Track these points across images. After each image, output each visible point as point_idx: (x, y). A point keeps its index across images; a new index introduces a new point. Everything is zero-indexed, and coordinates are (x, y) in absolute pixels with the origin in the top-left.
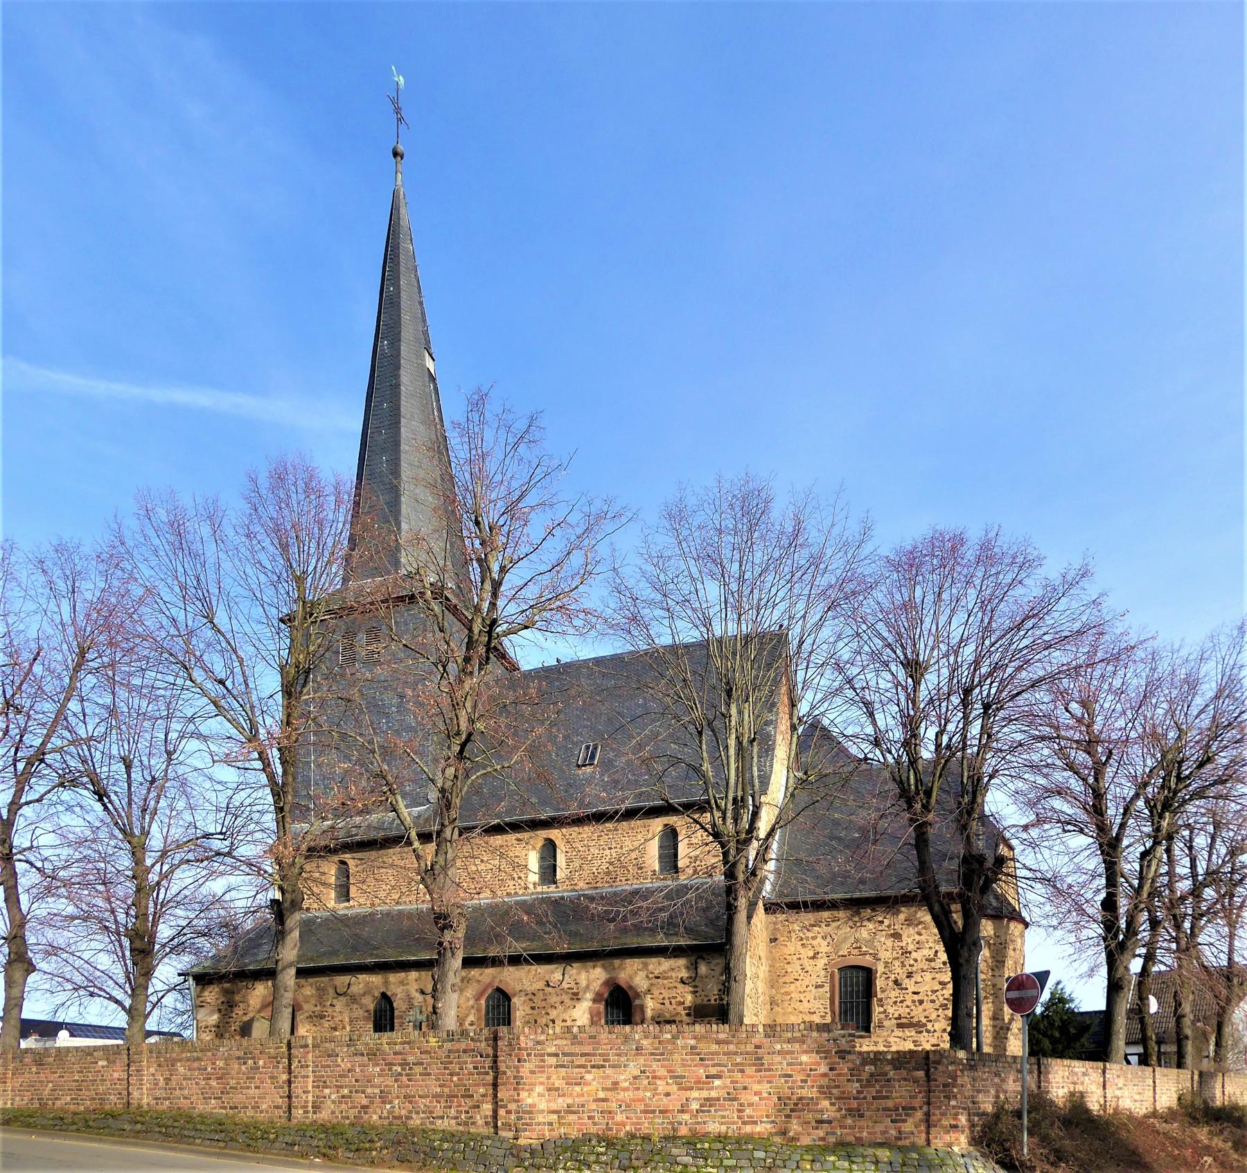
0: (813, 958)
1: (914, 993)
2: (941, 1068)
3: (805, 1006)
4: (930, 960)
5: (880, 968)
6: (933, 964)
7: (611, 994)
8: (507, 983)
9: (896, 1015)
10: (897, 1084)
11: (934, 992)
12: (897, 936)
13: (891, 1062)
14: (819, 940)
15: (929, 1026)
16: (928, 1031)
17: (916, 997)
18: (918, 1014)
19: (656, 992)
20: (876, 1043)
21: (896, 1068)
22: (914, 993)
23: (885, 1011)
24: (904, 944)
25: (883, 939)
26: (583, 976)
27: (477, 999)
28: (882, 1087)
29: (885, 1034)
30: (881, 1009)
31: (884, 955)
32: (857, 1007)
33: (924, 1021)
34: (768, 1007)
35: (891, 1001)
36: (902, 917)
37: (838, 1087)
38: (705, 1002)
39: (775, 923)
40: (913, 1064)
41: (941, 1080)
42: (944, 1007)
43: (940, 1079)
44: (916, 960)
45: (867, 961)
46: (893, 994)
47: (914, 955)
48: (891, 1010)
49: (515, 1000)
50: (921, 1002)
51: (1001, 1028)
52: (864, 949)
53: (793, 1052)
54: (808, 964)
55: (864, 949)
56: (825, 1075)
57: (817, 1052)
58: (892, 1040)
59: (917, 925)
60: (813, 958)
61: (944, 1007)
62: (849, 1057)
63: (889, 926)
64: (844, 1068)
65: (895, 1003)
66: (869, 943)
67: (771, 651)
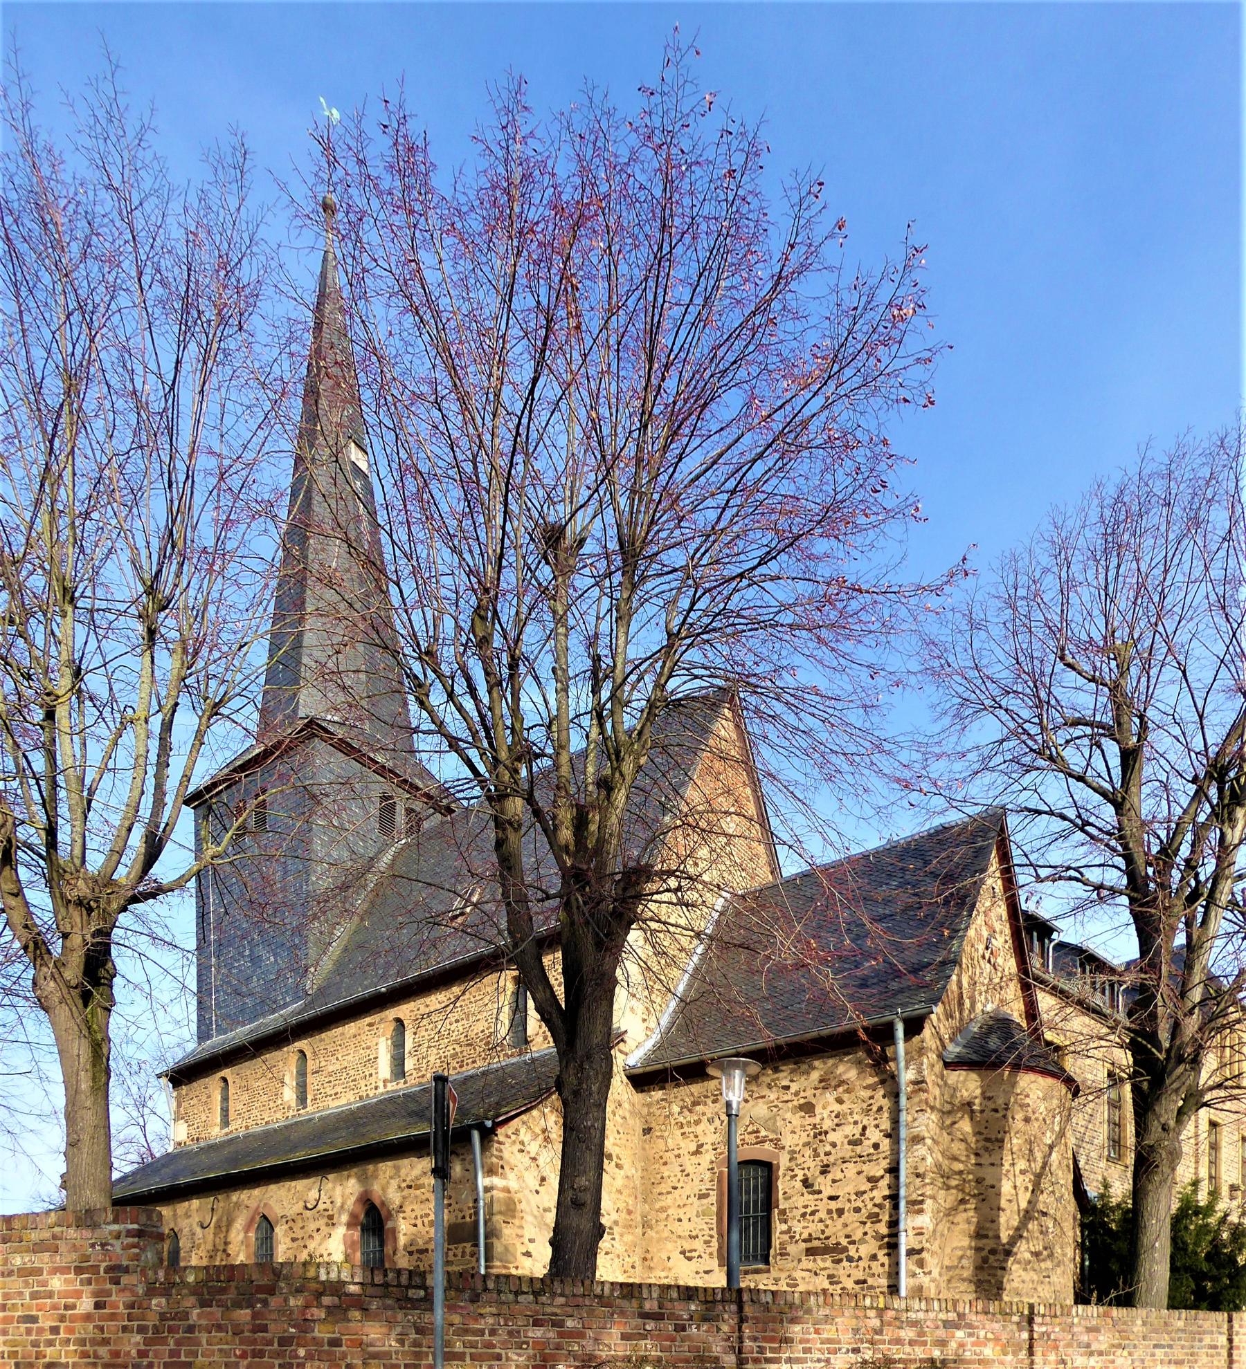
0: (697, 1152)
1: (831, 1198)
2: (274, 1302)
4: (854, 1143)
5: (783, 1161)
6: (858, 1149)
7: (367, 1214)
8: (271, 1208)
9: (805, 1236)
10: (204, 1337)
11: (859, 1194)
12: (808, 1108)
13: (196, 1290)
14: (704, 1125)
15: (852, 1251)
16: (850, 1259)
17: (834, 1205)
18: (836, 1232)
19: (407, 1208)
20: (777, 1280)
21: (204, 1304)
22: (831, 1198)
23: (789, 1231)
24: (817, 1120)
25: (789, 1116)
26: (339, 1190)
27: (246, 1232)
28: (178, 1343)
29: (790, 1265)
30: (784, 1227)
31: (788, 1141)
32: (755, 1224)
33: (844, 1242)
34: (639, 1230)
35: (797, 1213)
36: (815, 1075)
37: (106, 1342)
38: (460, 1221)
39: (649, 1105)
40: (232, 1294)
41: (275, 1330)
42: (874, 1218)
43: (271, 1327)
44: (834, 1145)
45: (764, 1152)
46: (800, 1201)
47: (832, 1137)
48: (797, 1228)
49: (277, 1230)
50: (840, 1212)
51: (993, 1252)
52: (763, 1133)
53: (39, 1271)
54: (689, 1163)
55: (763, 1133)
56: (87, 1317)
57: (79, 1270)
58: (798, 1274)
59: (836, 1087)
60: (697, 1152)
61: (874, 1218)
62: (125, 1280)
63: (797, 1094)
64: (119, 1300)
65: (804, 1215)
66: (770, 1123)
67: (988, 836)
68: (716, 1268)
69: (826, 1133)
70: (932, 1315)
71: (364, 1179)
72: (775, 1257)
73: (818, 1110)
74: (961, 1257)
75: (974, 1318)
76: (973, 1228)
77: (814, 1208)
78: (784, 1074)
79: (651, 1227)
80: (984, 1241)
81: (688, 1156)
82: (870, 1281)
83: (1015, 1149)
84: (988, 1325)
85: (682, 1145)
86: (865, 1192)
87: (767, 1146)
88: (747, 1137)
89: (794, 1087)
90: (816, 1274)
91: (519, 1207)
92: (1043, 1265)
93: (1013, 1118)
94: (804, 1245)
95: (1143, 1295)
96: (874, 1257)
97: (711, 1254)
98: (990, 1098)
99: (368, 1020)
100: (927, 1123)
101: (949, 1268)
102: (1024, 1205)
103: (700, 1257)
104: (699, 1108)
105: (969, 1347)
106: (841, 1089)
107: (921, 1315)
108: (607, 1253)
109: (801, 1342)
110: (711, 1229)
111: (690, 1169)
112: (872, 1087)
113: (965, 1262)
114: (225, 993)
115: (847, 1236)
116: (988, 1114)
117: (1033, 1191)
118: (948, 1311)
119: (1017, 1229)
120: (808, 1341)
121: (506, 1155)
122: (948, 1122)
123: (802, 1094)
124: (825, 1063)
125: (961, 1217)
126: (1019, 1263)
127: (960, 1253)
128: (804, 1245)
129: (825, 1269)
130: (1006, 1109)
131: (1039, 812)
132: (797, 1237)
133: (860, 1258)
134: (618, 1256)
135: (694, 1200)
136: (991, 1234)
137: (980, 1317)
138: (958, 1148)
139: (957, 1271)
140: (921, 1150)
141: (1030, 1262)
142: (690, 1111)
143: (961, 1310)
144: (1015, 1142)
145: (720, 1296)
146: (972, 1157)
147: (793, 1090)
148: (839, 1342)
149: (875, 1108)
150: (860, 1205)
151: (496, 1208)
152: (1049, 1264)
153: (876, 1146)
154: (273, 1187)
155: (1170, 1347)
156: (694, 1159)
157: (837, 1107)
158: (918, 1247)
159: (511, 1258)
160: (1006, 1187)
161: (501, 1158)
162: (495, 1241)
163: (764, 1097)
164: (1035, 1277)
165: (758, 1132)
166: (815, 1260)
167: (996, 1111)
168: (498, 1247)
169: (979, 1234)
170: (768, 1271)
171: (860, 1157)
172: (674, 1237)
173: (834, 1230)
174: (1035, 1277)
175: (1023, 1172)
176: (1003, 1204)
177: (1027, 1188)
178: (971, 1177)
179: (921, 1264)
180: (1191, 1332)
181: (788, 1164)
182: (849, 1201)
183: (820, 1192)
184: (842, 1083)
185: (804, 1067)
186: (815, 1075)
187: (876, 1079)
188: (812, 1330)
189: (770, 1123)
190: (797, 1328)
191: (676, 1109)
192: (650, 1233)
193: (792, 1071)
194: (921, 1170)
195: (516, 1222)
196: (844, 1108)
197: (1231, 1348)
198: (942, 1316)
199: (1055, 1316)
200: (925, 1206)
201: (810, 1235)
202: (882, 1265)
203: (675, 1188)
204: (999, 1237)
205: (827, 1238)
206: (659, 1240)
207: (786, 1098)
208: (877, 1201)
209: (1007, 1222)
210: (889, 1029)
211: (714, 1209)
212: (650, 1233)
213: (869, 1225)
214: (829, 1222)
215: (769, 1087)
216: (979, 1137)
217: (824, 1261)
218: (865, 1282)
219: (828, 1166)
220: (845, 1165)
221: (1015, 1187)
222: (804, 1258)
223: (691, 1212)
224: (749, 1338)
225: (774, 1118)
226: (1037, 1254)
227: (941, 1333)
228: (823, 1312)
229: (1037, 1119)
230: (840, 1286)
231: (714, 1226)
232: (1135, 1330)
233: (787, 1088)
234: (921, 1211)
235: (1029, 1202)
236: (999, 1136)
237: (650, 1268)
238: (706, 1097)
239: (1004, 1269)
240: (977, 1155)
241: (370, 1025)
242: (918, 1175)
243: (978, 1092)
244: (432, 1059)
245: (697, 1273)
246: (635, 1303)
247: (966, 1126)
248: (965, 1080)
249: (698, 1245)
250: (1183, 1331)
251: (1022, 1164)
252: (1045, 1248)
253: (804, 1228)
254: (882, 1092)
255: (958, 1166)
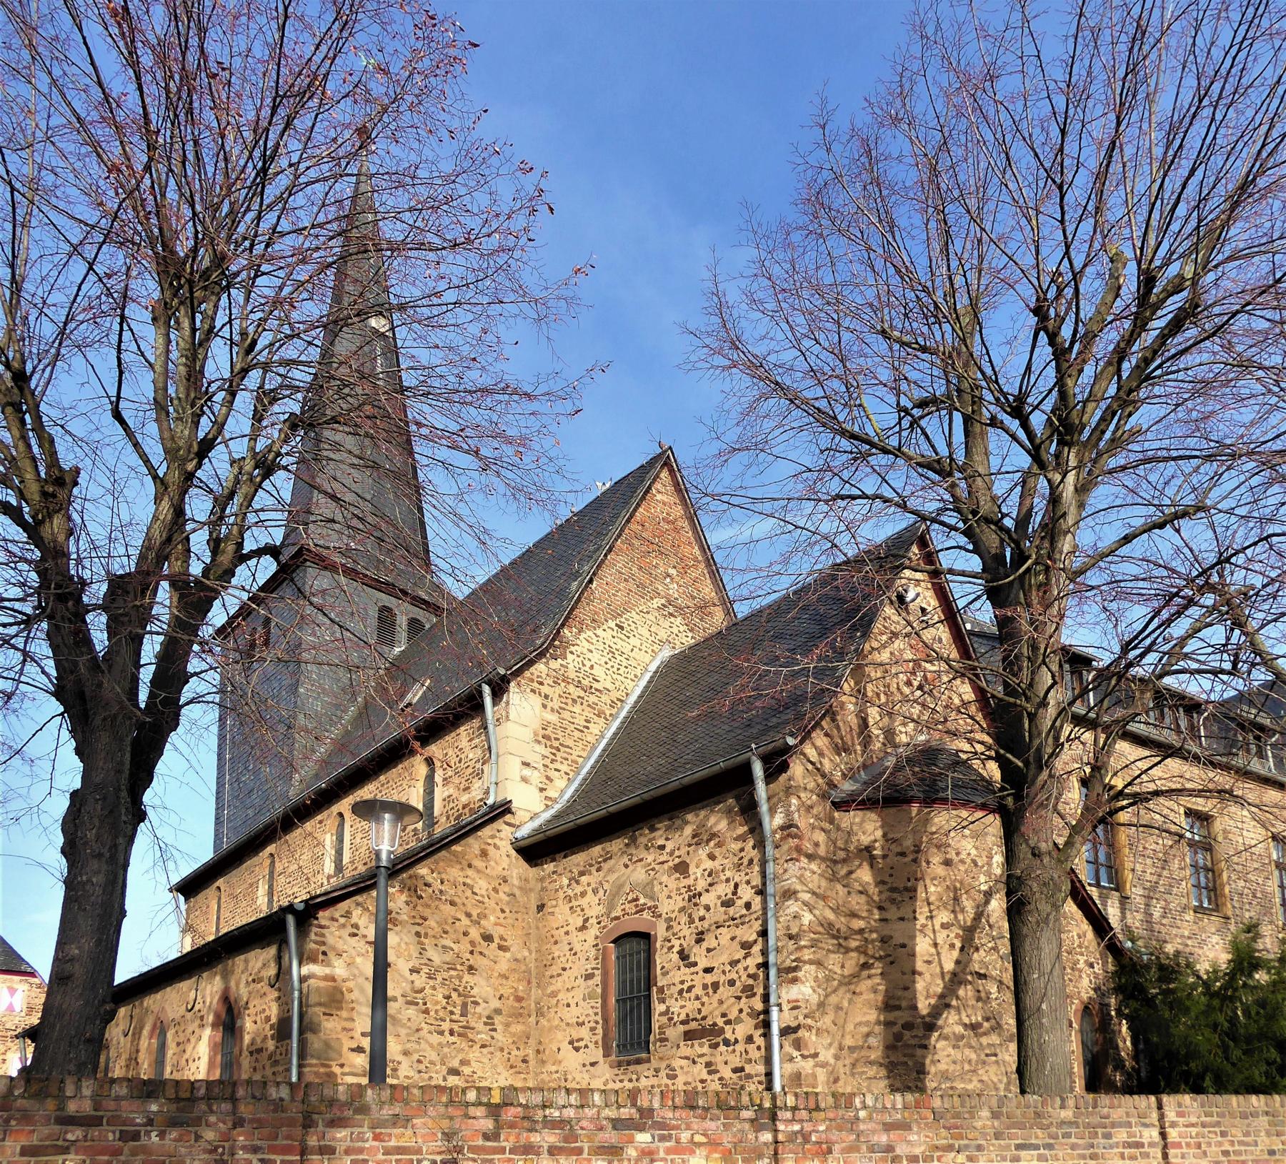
0: (583, 928)
1: (708, 970)
3: (571, 1015)
4: (727, 904)
5: (660, 931)
6: (731, 911)
9: (683, 1017)
11: (734, 963)
16: (727, 1043)
17: (709, 979)
18: (712, 1011)
22: (708, 970)
23: (667, 1012)
24: (690, 881)
25: (664, 878)
26: (209, 987)
31: (666, 907)
36: (688, 830)
39: (542, 880)
42: (749, 991)
44: (707, 908)
46: (676, 976)
47: (705, 899)
50: (716, 986)
51: (908, 1026)
52: (642, 901)
54: (576, 938)
55: (642, 901)
58: (677, 1063)
59: (708, 841)
60: (583, 928)
63: (671, 854)
66: (648, 889)
68: (601, 1060)
69: (700, 894)
70: (589, 1112)
71: (226, 977)
72: (655, 1045)
73: (692, 869)
74: (868, 1035)
75: (670, 1115)
76: (880, 998)
77: (690, 984)
78: (660, 832)
79: (542, 1015)
80: (897, 1013)
81: (575, 933)
82: (748, 1069)
83: (932, 899)
84: (696, 1124)
85: (571, 921)
86: (738, 961)
87: (646, 915)
88: (627, 906)
89: (670, 846)
90: (694, 1062)
91: (348, 996)
92: (984, 1040)
93: (928, 863)
94: (682, 1028)
95: (1034, 1075)
96: (750, 1039)
97: (596, 1043)
98: (895, 841)
99: (319, 817)
100: (803, 875)
101: (852, 1049)
102: (949, 966)
103: (586, 1046)
104: (583, 879)
105: (662, 1154)
106: (712, 843)
107: (570, 1113)
108: (483, 1046)
109: (347, 1152)
110: (596, 1014)
111: (577, 947)
112: (742, 838)
113: (873, 1041)
114: (235, 807)
115: (724, 1015)
116: (893, 859)
117: (962, 949)
118: (619, 1107)
119: (942, 996)
120: (361, 1151)
121: (330, 940)
122: (843, 872)
123: (677, 853)
124: (697, 816)
125: (864, 985)
126: (946, 1038)
127: (865, 1030)
128: (682, 1028)
129: (703, 1055)
130: (918, 851)
131: (853, 498)
132: (676, 1019)
133: (736, 1041)
134: (502, 1050)
135: (580, 981)
136: (904, 1004)
137: (683, 1113)
138: (857, 902)
139: (863, 1053)
140: (792, 907)
141: (963, 1037)
142: (578, 882)
143: (646, 1104)
144: (932, 890)
145: (203, 1091)
146: (876, 911)
147: (668, 850)
148: (419, 1151)
149: (745, 861)
150: (734, 976)
151: (313, 999)
152: (994, 1039)
153: (748, 906)
154: (168, 989)
155: (1049, 1147)
156: (581, 936)
157: (709, 864)
158: (794, 1024)
159: (333, 1055)
160: (922, 946)
161: (324, 943)
162: (309, 1036)
163: (641, 860)
164: (973, 1056)
165: (637, 899)
166: (692, 1046)
167: (903, 854)
168: (315, 1042)
169: (889, 1005)
170: (649, 1061)
171: (734, 919)
172: (563, 1024)
173: (711, 1008)
174: (973, 1056)
175: (944, 926)
176: (920, 966)
177: (952, 946)
178: (874, 936)
179: (798, 1045)
180: (1088, 1125)
181: (666, 934)
182: (724, 972)
183: (695, 964)
184: (713, 836)
185: (678, 822)
186: (688, 830)
187: (746, 828)
188: (369, 1135)
189: (648, 889)
190: (341, 1134)
191: (566, 881)
192: (543, 1022)
193: (668, 829)
194: (794, 931)
195: (344, 1014)
196: (716, 865)
197: (1165, 1147)
198: (610, 1113)
199: (817, 1109)
200: (800, 974)
201: (687, 1015)
202: (759, 1048)
203: (564, 969)
204: (915, 1008)
205: (704, 1018)
206: (550, 1029)
207: (662, 859)
208: (752, 970)
209: (926, 990)
210: (746, 768)
211: (599, 990)
212: (543, 1022)
213: (744, 1000)
214: (705, 999)
215: (647, 848)
216: (882, 887)
217: (701, 1045)
218: (742, 1069)
219: (702, 933)
220: (720, 930)
221: (936, 945)
222: (682, 1044)
223: (578, 994)
224: (244, 1148)
225: (651, 883)
226: (974, 1027)
227: (610, 1136)
228: (387, 1112)
229: (962, 861)
230: (718, 1075)
231: (599, 1010)
232: (979, 1124)
233: (662, 847)
234: (795, 980)
235: (958, 962)
236: (909, 884)
237: (543, 1062)
238: (591, 865)
239: (925, 1047)
240: (880, 908)
241: (321, 822)
242: (791, 937)
243: (879, 833)
244: (362, 850)
245: (584, 1065)
246: (51, 1104)
247: (865, 875)
248: (863, 821)
249: (584, 1032)
250: (1070, 1123)
251: (944, 916)
252: (988, 1019)
253: (682, 1007)
254: (751, 843)
255: (858, 924)
